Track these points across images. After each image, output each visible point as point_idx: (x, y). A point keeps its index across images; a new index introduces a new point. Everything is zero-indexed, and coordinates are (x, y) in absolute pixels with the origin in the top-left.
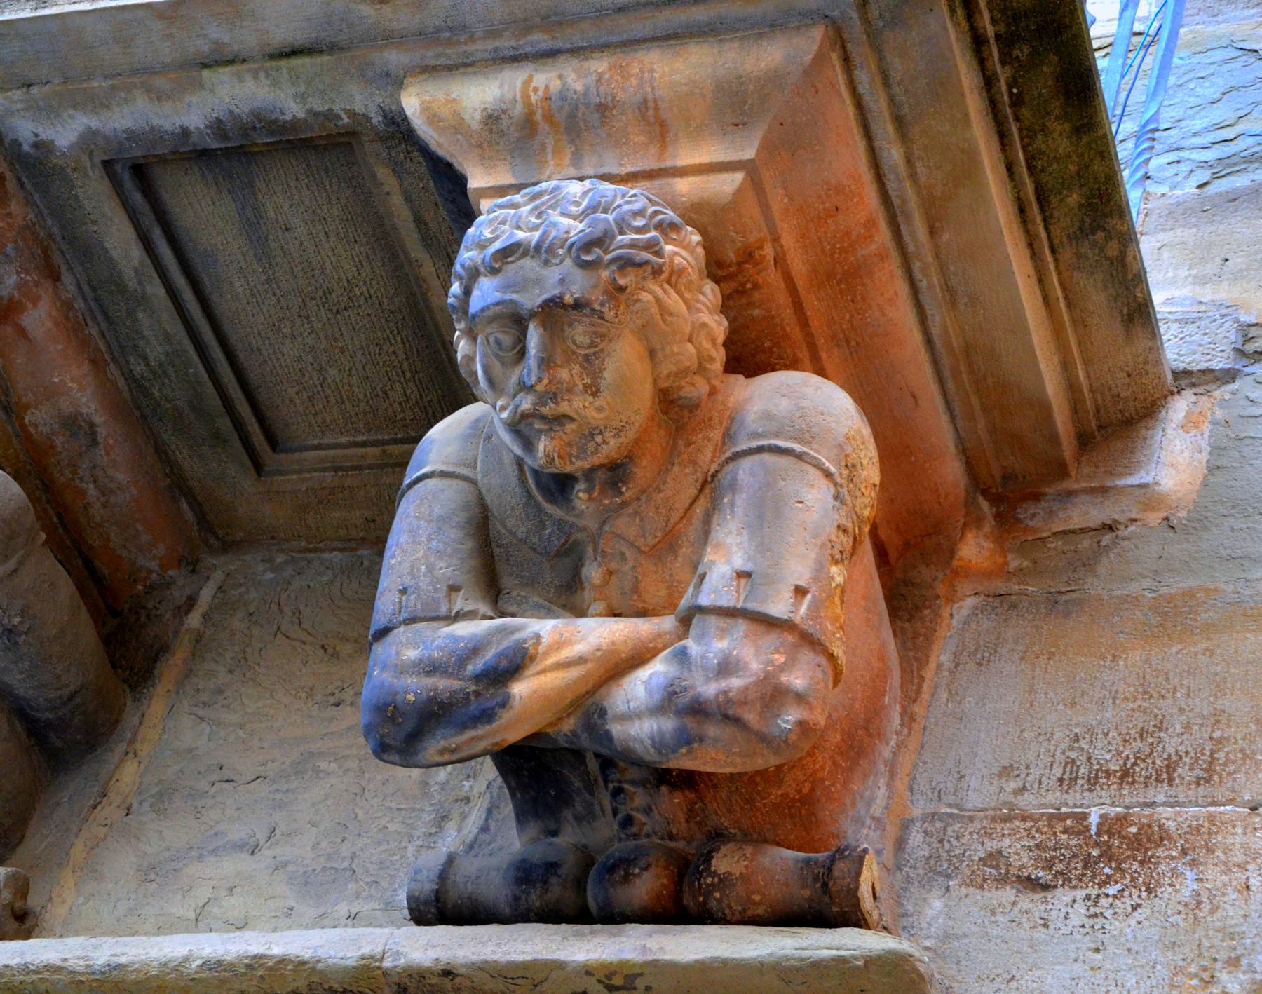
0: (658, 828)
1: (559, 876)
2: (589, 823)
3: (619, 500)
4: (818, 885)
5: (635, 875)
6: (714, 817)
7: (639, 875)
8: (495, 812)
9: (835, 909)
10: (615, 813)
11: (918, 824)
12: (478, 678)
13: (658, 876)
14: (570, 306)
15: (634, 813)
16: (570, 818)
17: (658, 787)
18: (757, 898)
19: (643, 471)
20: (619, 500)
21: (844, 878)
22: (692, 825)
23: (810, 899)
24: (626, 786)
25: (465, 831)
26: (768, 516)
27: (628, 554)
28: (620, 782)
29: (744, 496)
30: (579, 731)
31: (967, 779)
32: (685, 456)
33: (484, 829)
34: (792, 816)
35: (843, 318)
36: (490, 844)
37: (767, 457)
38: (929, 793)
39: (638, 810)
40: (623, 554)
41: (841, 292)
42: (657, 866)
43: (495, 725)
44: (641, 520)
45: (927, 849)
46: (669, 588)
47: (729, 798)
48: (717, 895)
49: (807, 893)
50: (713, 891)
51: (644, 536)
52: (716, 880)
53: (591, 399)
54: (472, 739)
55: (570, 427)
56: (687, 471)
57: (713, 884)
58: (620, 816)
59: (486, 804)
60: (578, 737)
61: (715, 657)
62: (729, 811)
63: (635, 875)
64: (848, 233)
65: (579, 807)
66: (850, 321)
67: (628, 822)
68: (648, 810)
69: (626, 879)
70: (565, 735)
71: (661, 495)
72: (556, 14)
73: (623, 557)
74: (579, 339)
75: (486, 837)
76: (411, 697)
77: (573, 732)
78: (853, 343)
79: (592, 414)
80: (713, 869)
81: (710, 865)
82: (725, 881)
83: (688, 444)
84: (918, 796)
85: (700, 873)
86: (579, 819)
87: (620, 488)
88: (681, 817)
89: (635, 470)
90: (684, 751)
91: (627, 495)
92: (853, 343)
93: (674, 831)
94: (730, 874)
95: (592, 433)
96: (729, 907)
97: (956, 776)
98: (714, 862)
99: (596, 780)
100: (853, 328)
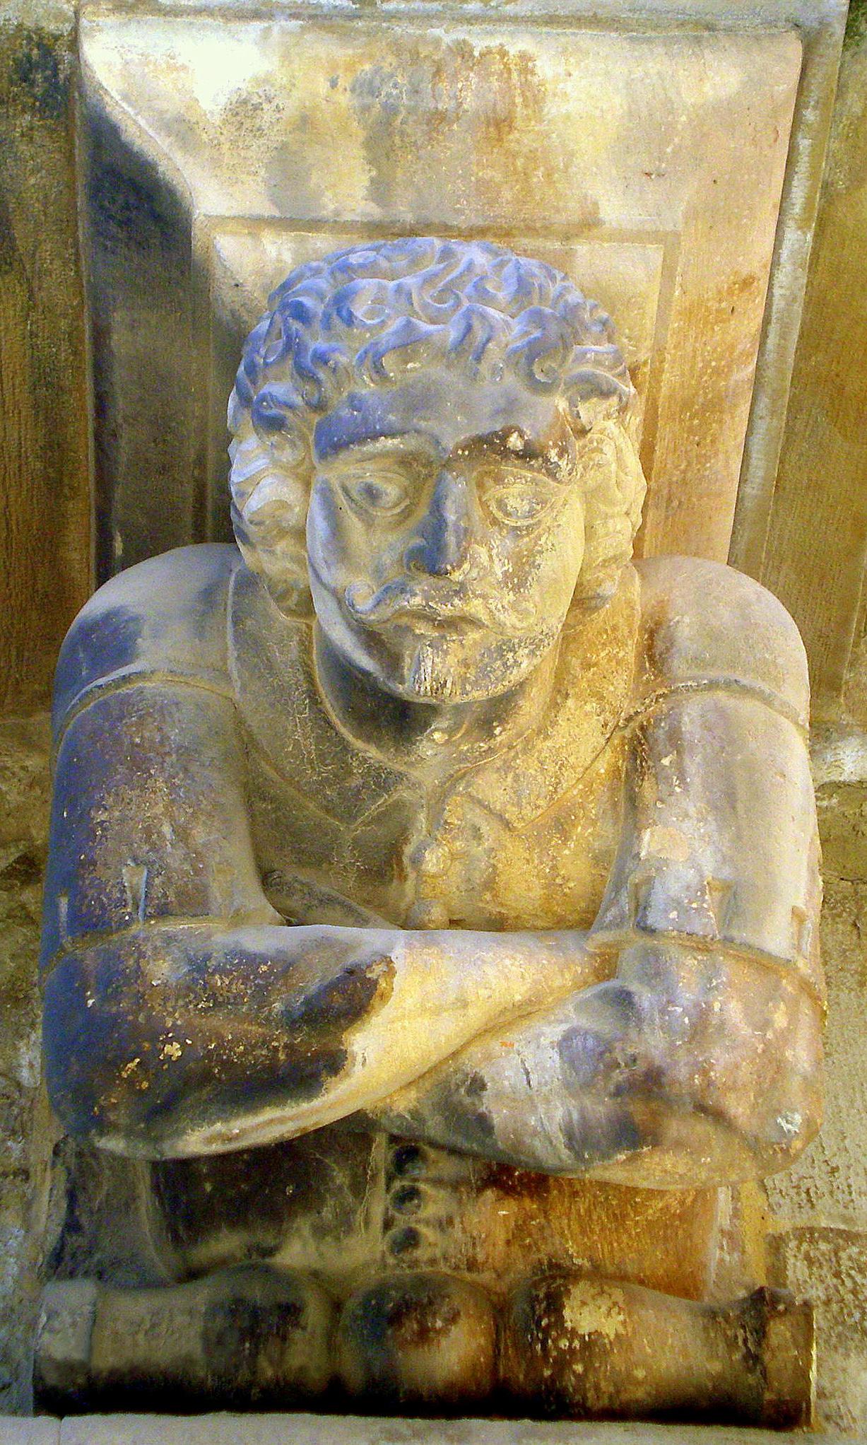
0: (452, 1251)
1: (304, 1328)
2: (338, 1239)
3: (484, 746)
4: (737, 1356)
5: (438, 1332)
6: (557, 1239)
7: (444, 1331)
8: (81, 1198)
9: (768, 1396)
10: (388, 1224)
11: (793, 1244)
12: (293, 1022)
13: (472, 1333)
14: (516, 453)
15: (423, 1230)
16: (306, 1231)
17: (480, 1190)
18: (640, 1374)
19: (530, 708)
20: (484, 746)
21: (787, 1349)
22: (515, 1249)
23: (721, 1377)
24: (422, 1186)
25: (40, 1227)
26: (737, 800)
27: (485, 829)
28: (416, 1180)
29: (698, 759)
30: (426, 1112)
31: (842, 1171)
32: (584, 684)
33: (72, 1226)
34: (666, 1239)
35: (677, 467)
36: (90, 1253)
37: (721, 695)
38: (792, 1192)
39: (427, 1223)
40: (476, 829)
41: (691, 430)
42: (469, 1316)
43: (316, 1102)
44: (516, 779)
45: (821, 1287)
46: (547, 886)
47: (589, 1212)
48: (579, 1368)
49: (715, 1367)
50: (570, 1364)
51: (519, 805)
52: (576, 1344)
53: (511, 597)
54: (271, 1121)
55: (473, 636)
56: (588, 708)
57: (571, 1350)
58: (393, 1231)
59: (62, 1187)
60: (423, 1121)
61: (686, 1012)
62: (583, 1232)
63: (438, 1332)
64: (732, 347)
65: (327, 1213)
66: (684, 472)
67: (410, 1239)
68: (444, 1224)
69: (424, 1335)
70: (400, 1116)
71: (549, 743)
72: (773, 35)
73: (477, 834)
74: (512, 503)
75: (74, 1241)
76: (174, 1050)
77: (415, 1114)
78: (676, 503)
79: (509, 619)
80: (568, 1325)
81: (561, 1319)
82: (591, 1346)
83: (587, 666)
84: (775, 1198)
85: (546, 1331)
86: (320, 1231)
87: (492, 729)
88: (501, 1235)
89: (521, 703)
90: (621, 1157)
91: (499, 739)
92: (676, 503)
93: (481, 1257)
94: (600, 1334)
95: (504, 648)
96: (597, 1388)
97: (825, 1168)
98: (567, 1313)
99: (374, 1177)
100: (684, 482)
